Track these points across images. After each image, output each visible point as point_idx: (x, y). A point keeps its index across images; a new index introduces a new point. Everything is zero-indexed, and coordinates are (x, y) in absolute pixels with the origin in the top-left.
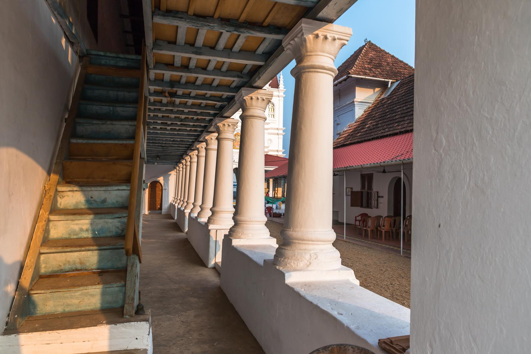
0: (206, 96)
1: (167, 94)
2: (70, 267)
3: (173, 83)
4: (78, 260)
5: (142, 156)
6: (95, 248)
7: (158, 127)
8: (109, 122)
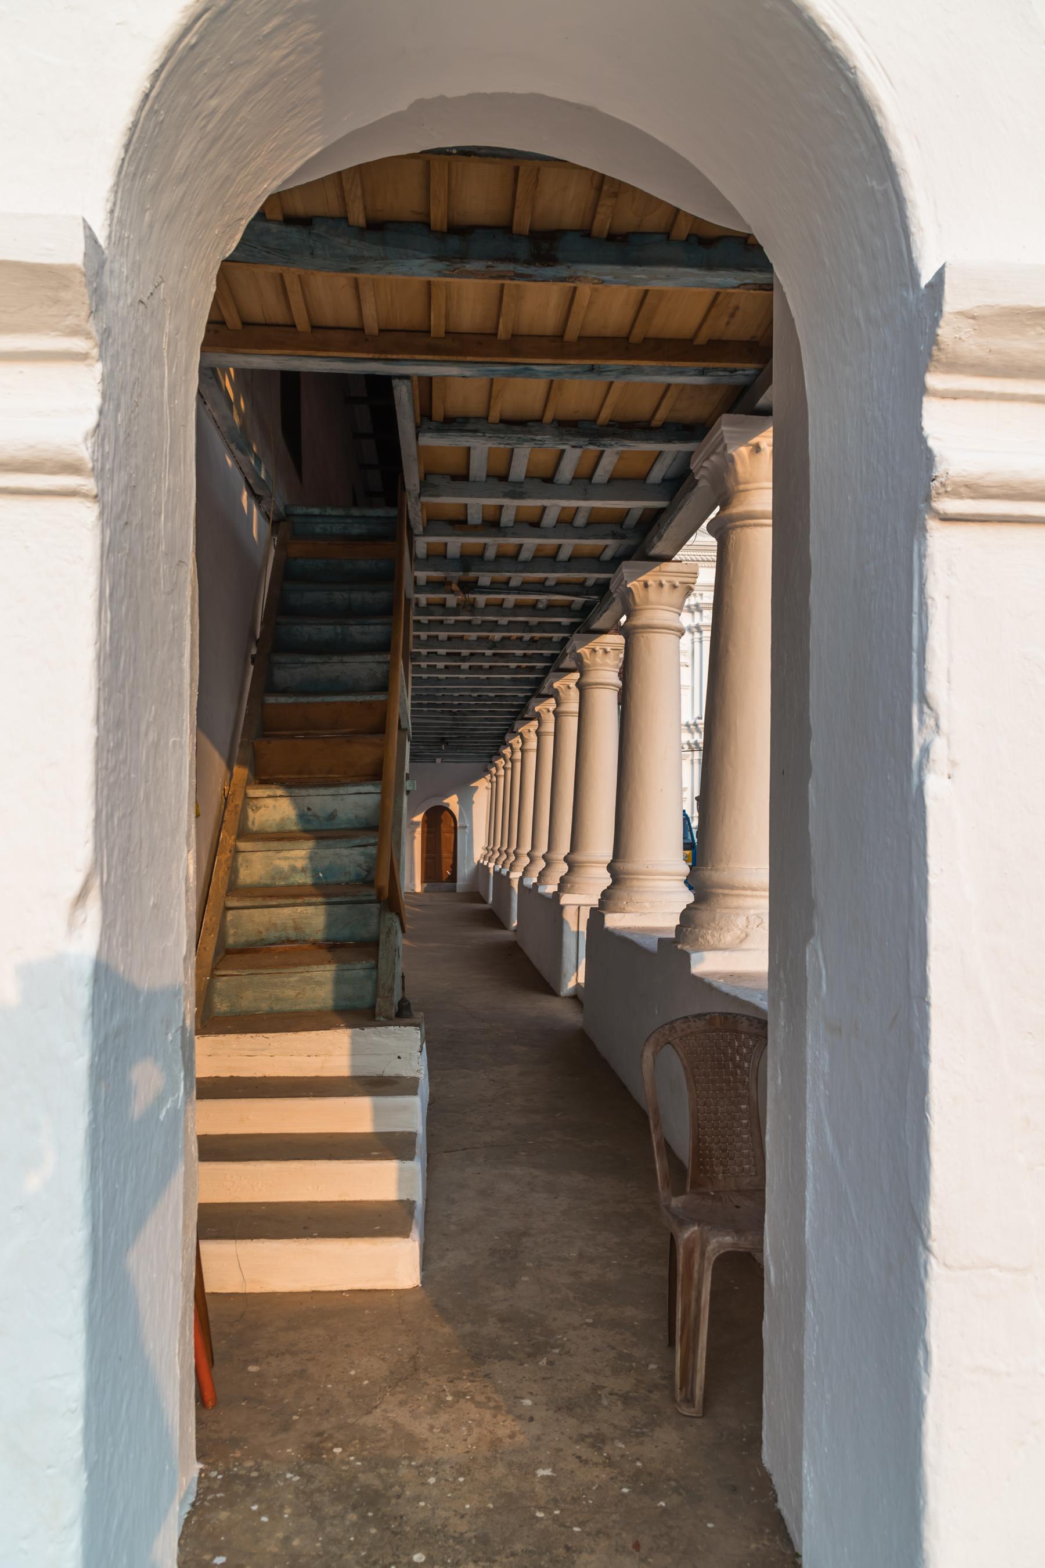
0: (547, 583)
1: (455, 587)
2: (277, 934)
3: (469, 560)
4: (290, 923)
5: (403, 726)
6: (320, 899)
7: (441, 665)
8: (335, 659)
